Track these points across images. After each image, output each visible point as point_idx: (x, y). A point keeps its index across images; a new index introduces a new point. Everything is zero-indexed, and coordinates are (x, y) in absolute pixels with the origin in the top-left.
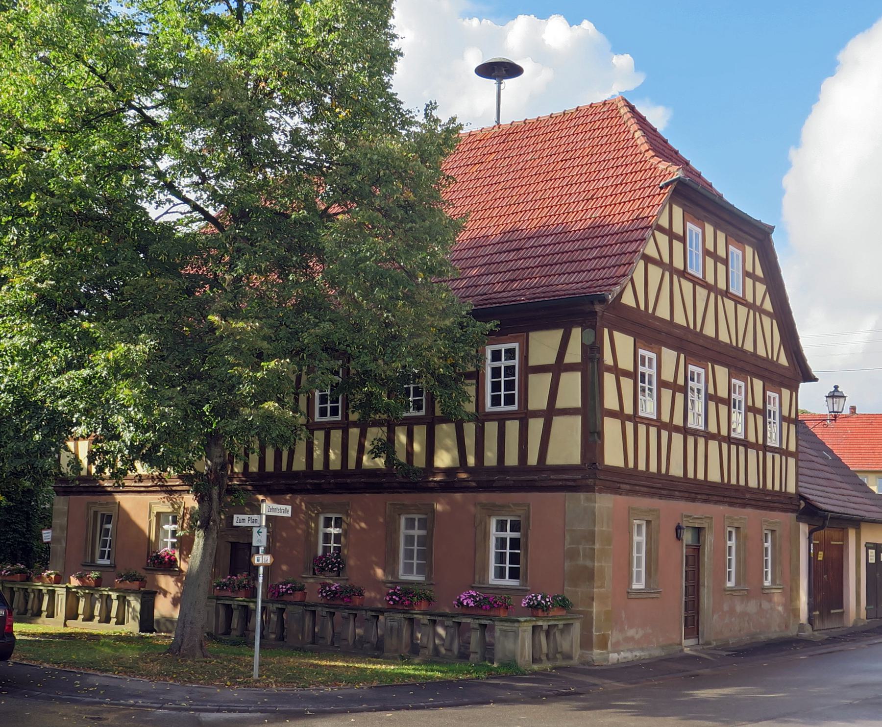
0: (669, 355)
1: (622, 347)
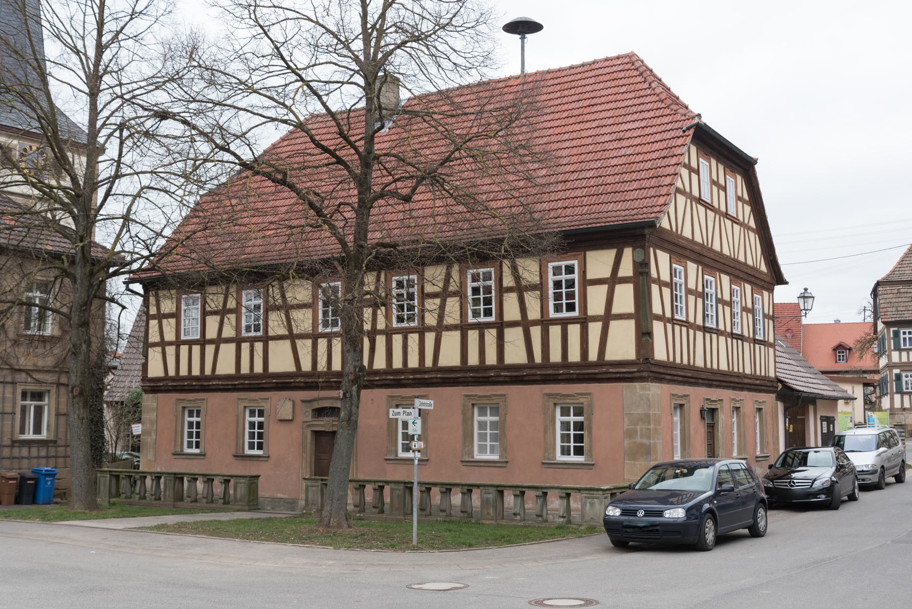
0: (692, 267)
1: (662, 263)
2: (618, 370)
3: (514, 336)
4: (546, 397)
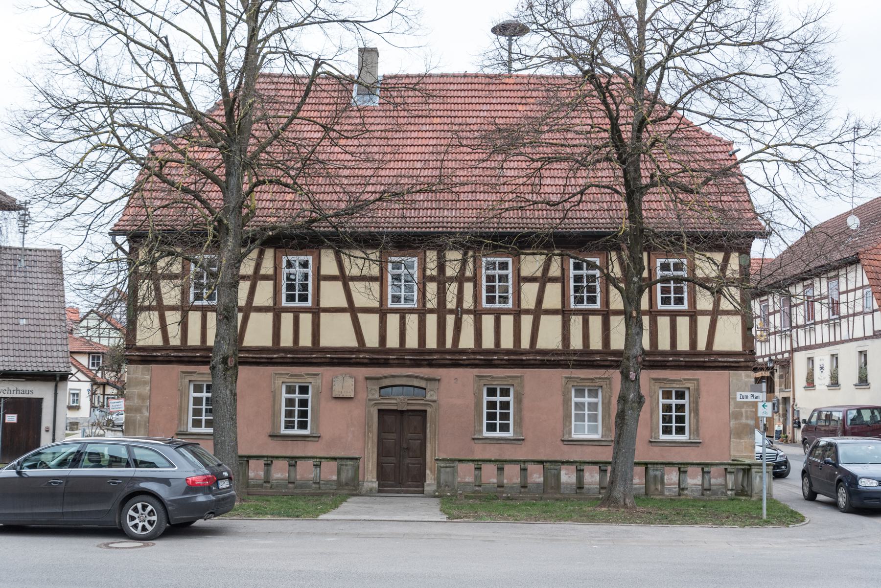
2: (725, 359)
3: (618, 324)
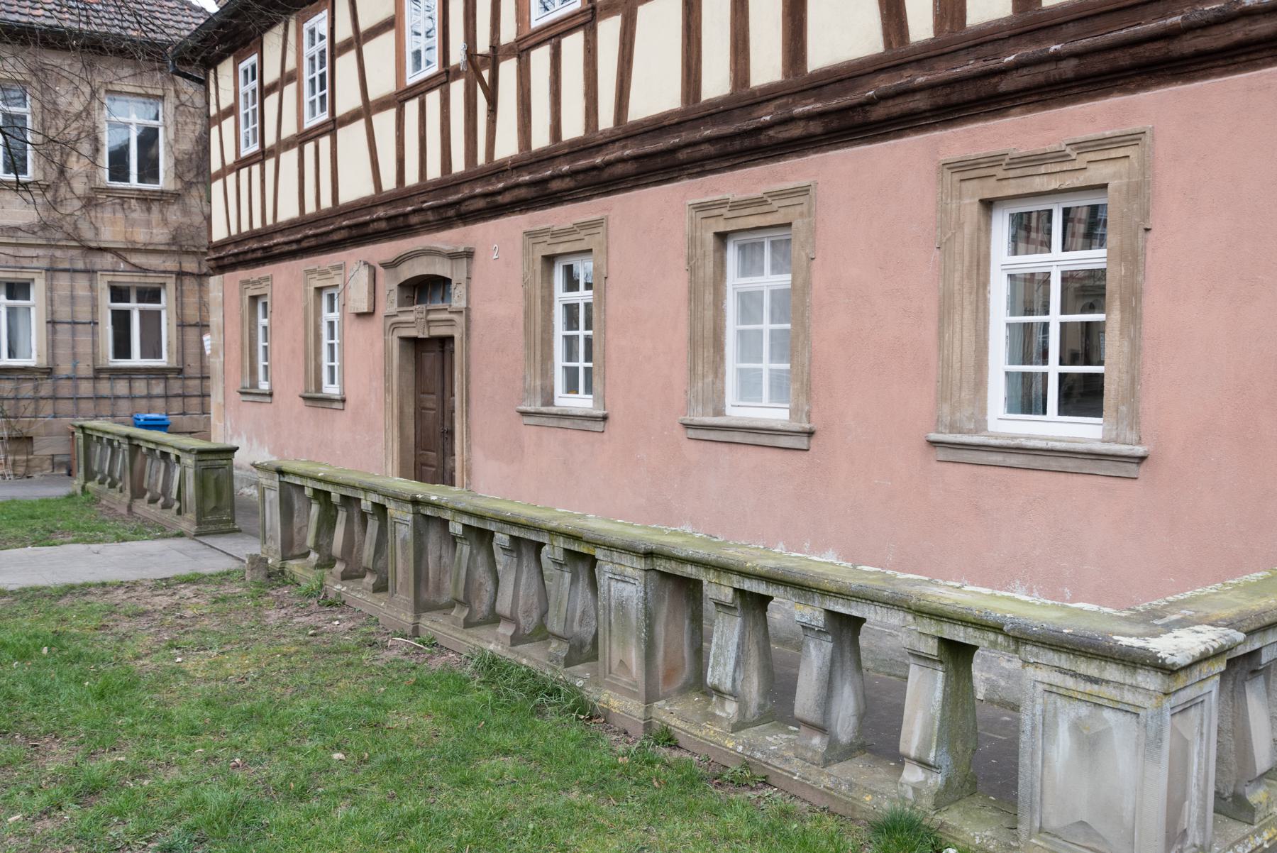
4: (951, 178)
